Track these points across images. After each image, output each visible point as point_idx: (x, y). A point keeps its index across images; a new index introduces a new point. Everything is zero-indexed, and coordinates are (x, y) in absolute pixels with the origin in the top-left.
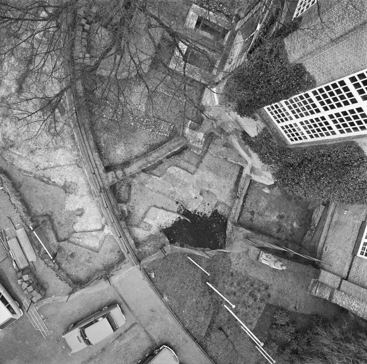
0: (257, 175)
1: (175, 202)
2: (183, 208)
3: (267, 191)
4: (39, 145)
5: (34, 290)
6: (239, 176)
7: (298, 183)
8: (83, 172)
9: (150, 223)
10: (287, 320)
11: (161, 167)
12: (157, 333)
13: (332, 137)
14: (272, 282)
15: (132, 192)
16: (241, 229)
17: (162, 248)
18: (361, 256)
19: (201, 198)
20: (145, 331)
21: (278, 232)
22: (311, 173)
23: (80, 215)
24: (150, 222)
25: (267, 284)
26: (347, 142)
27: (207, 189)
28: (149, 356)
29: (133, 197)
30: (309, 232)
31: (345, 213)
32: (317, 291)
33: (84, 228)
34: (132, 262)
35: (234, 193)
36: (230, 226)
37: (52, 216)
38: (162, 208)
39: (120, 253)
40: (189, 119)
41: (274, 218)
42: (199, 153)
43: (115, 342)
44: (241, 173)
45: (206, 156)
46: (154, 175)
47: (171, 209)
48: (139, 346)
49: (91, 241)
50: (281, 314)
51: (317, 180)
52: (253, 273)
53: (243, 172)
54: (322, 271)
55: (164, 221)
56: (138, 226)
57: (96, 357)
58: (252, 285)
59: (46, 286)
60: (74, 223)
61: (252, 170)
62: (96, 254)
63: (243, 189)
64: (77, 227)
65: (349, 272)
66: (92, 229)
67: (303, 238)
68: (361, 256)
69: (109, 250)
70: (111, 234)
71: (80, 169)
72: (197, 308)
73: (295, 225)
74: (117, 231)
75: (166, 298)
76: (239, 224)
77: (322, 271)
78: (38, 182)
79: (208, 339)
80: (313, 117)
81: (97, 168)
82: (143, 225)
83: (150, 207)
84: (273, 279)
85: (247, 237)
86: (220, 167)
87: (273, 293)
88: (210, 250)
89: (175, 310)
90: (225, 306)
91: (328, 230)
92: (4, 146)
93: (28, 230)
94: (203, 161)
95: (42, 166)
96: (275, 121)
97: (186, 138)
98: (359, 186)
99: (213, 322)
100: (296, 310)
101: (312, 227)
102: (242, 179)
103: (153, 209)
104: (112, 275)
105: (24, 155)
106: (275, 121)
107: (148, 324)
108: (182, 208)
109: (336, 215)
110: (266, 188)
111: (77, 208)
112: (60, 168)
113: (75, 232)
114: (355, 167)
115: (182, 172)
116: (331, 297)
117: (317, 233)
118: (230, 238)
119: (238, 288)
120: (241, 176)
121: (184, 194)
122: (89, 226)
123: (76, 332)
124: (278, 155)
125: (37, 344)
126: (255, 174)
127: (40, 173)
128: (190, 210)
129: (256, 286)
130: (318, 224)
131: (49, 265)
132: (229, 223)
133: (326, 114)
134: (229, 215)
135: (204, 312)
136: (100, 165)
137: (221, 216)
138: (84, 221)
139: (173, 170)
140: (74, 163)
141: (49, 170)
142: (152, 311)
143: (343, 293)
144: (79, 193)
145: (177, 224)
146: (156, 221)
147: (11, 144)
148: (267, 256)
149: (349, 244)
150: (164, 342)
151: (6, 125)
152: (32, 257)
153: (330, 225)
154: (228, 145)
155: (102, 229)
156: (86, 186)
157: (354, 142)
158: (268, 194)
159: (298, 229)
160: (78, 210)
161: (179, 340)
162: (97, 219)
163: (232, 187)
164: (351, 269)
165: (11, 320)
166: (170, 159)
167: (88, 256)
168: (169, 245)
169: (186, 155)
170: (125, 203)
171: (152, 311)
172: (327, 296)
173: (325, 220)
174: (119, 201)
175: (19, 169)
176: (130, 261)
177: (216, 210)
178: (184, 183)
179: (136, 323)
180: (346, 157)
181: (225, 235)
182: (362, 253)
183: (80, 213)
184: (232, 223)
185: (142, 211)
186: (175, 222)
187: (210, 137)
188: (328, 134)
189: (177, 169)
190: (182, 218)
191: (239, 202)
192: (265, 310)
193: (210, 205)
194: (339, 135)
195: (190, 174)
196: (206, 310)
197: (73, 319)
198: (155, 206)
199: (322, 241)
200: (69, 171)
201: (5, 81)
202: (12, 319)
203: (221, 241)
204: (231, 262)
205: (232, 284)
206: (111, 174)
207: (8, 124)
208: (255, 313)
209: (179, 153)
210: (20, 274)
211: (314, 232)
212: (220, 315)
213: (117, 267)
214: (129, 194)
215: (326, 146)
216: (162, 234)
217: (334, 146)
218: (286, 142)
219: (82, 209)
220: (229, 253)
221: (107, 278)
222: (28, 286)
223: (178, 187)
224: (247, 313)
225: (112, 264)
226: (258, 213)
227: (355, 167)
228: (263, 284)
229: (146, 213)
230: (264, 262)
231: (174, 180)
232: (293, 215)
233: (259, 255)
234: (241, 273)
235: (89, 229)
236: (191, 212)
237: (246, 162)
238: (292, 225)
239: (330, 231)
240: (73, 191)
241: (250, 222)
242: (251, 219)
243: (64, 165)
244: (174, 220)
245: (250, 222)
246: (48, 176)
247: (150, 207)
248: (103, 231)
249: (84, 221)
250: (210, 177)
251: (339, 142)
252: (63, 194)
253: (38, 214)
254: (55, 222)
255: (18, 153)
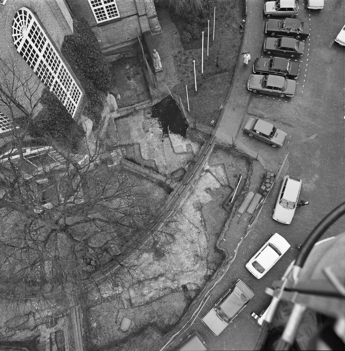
0: (113, 107)
1: (163, 142)
2: (163, 136)
3: (119, 96)
4: (185, 241)
5: (267, 178)
6: (122, 117)
7: (102, 72)
8: (183, 205)
9: (185, 147)
10: (185, 32)
11: (148, 165)
12: (244, 99)
13: (65, 67)
14: (171, 56)
15: (175, 170)
16: (152, 94)
17: (194, 129)
18: (119, 14)
19: (150, 129)
20: (248, 106)
21: (139, 74)
22: (92, 67)
23: (209, 189)
24: (185, 147)
25: (173, 58)
26: (63, 55)
27: (142, 130)
28: (261, 94)
29: (177, 167)
30: (126, 56)
31: (100, 41)
32: (157, 27)
33: (215, 182)
34: (214, 139)
35: (134, 113)
36: (155, 102)
37: (221, 204)
38: (172, 147)
39: (215, 151)
40: (108, 168)
41: (132, 81)
42: (124, 149)
43: (266, 117)
44: (119, 118)
45: (123, 144)
46: (156, 165)
47: (169, 142)
48: (259, 103)
49: (220, 172)
50: (184, 39)
51: (93, 60)
52: (173, 69)
53: (117, 117)
54: (143, 31)
55: (178, 140)
56: (192, 152)
57: (282, 122)
58: (180, 65)
59: (262, 176)
60: (217, 189)
61: (112, 111)
62: (225, 164)
63: (127, 110)
64: (218, 186)
65: (133, 15)
66: (212, 177)
67: (132, 58)
68: (119, 14)
69: (218, 159)
70: (207, 163)
71: (183, 209)
72: (215, 87)
73: (128, 67)
74: (202, 159)
75: (221, 107)
76: (150, 98)
77: (143, 31)
78: (207, 226)
79: (228, 69)
80: (61, 84)
81: (174, 196)
82: (190, 150)
83: (176, 154)
84: (168, 57)
85: (154, 87)
86: (124, 132)
87: (176, 51)
88: (177, 102)
89: (224, 97)
90: (202, 72)
91: (117, 45)
92: (201, 260)
93: (238, 208)
94: (127, 144)
95: (197, 230)
96: (75, 110)
97: (121, 161)
98: (82, 33)
99: (217, 73)
100: (177, 32)
101: (122, 56)
102: (122, 115)
103: (176, 151)
104: (230, 145)
105: (198, 245)
106: (75, 110)
107: (243, 106)
108: (164, 136)
109: (105, 46)
110: (118, 98)
111: (207, 194)
112: (191, 220)
113: (221, 185)
114: (74, 42)
115: (142, 150)
116: (154, 17)
117: (123, 50)
118: (162, 96)
119: (187, 72)
120: (121, 117)
121: (155, 140)
122: (212, 180)
123: (274, 140)
124: (94, 96)
125: (297, 158)
126: (114, 108)
127: (201, 229)
128: (162, 131)
129: (179, 63)
130: (117, 54)
131: (249, 183)
132: (153, 103)
133: (56, 76)
134: (149, 107)
135: (214, 81)
136: (171, 195)
137: (153, 112)
138: (212, 185)
139: (145, 156)
140: (182, 215)
141: (196, 225)
142: (234, 109)
143: (147, 11)
144: (197, 199)
145: (175, 131)
146: (182, 144)
147: (196, 257)
148: (156, 66)
149: (117, 26)
150: (247, 91)
151: (187, 268)
152: (251, 195)
153: (114, 46)
154: (108, 136)
155: (208, 171)
156: (191, 199)
157: (61, 51)
158: (120, 95)
159: (129, 64)
160: (207, 192)
161: (240, 84)
162: (205, 178)
163: (131, 117)
164: (130, 15)
165: (290, 178)
166: (140, 163)
167: (230, 167)
168: (190, 126)
169: (131, 156)
170: (184, 169)
171: (234, 109)
172: (155, 20)
173: (112, 51)
174: (185, 172)
175: (208, 242)
176: (214, 141)
177: (151, 117)
178: (149, 145)
179: (247, 114)
180: (72, 50)
181: (162, 101)
182: (117, 15)
183: (208, 191)
184: (152, 102)
185: (182, 157)
186: (175, 134)
187: (110, 149)
188: (65, 70)
189: (143, 154)
190: (170, 132)
191: (137, 106)
192: (189, 49)
193: (151, 122)
194: (62, 63)
195: (141, 145)
196: (212, 80)
197: (269, 149)
198: (174, 151)
199: (126, 45)
200: (188, 214)
201: (161, 287)
202: (290, 178)
203: (167, 100)
204: (176, 86)
205: (187, 77)
206: (172, 186)
207: (186, 267)
208: (195, 54)
209: (132, 160)
210: (265, 193)
211: (124, 53)
212: (210, 72)
213: (223, 146)
214: (177, 171)
215: (72, 68)
216: (187, 135)
217: (69, 62)
218: (83, 97)
219: (205, 191)
220: (171, 90)
221: (234, 146)
222: (267, 183)
223: (153, 146)
224: (198, 58)
225: (225, 151)
226: (136, 92)
227: (74, 42)
228: (175, 60)
229: (181, 154)
230: (161, 66)
231: (151, 152)
232: (123, 72)
233: (159, 72)
234: (178, 76)
235: (214, 179)
236: (163, 130)
237: (110, 118)
238: (129, 68)
239: (117, 43)
240: (199, 203)
241: (145, 93)
242: (142, 94)
243: (187, 219)
244: (174, 135)
245: (145, 93)
246: (200, 223)
247: (176, 154)
248: (209, 169)
249: (212, 185)
250: (135, 133)
251: (66, 61)
252: (205, 207)
253: (226, 212)
254: (224, 200)
255: (199, 249)
